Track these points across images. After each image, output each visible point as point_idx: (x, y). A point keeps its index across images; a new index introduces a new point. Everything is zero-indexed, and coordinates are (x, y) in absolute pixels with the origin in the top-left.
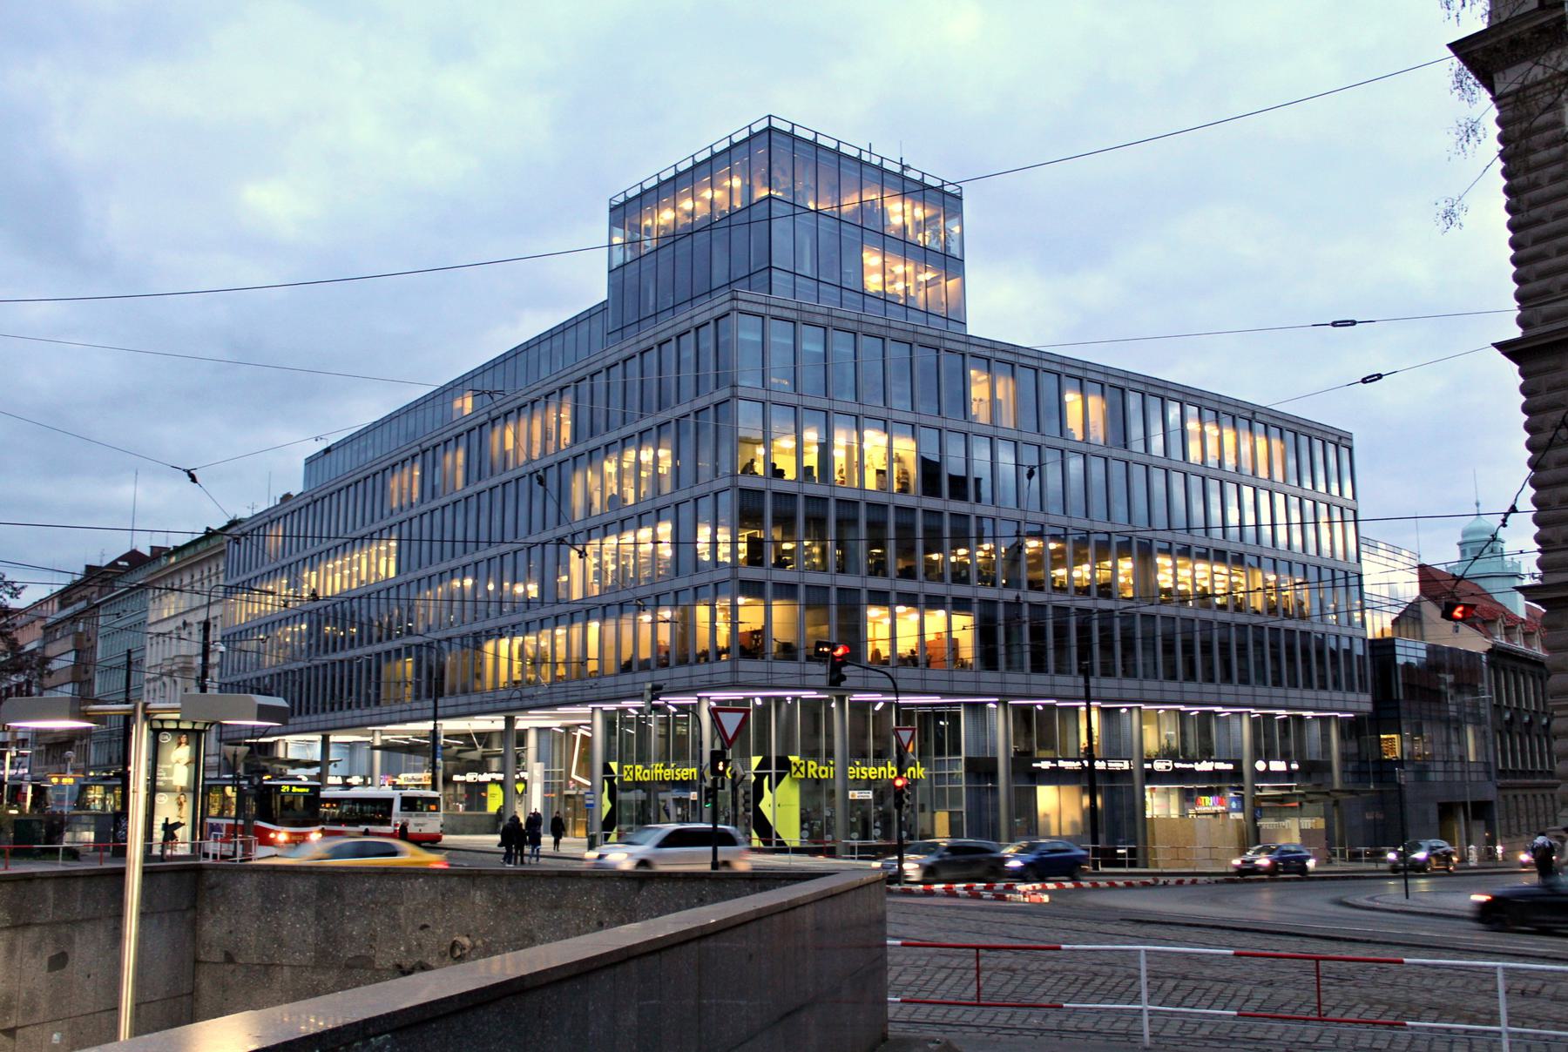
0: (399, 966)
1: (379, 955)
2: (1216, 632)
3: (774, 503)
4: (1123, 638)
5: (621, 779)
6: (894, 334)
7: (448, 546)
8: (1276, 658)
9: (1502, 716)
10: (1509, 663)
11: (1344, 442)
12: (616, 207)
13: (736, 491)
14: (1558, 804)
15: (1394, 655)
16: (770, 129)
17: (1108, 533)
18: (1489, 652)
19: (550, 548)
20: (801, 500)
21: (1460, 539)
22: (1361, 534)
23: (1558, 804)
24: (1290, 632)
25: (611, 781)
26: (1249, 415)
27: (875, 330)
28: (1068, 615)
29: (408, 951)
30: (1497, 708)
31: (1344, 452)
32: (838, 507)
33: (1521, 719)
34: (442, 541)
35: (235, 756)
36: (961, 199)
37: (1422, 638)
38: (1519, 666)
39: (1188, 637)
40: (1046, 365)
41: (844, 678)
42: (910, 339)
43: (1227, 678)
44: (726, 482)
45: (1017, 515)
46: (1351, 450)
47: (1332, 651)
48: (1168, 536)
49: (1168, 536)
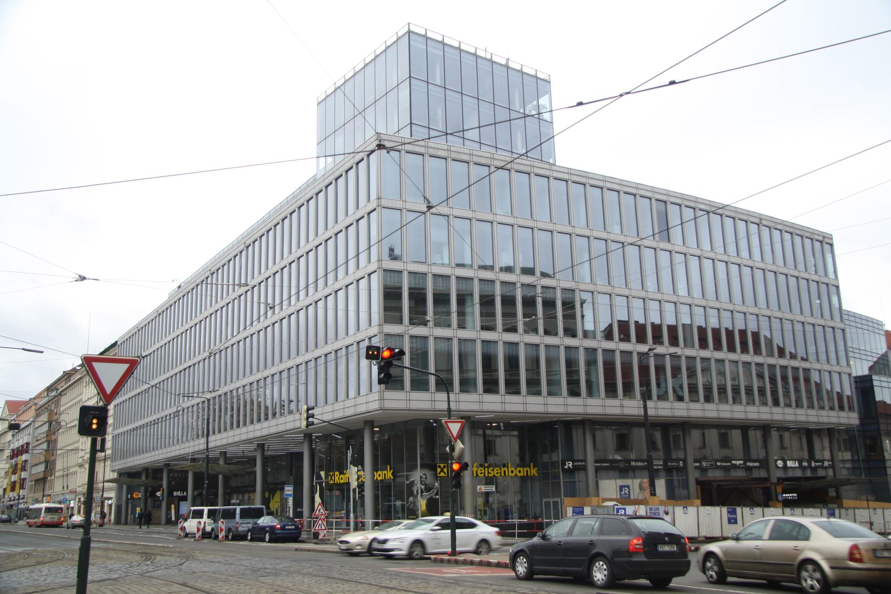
5: (327, 483)
11: (827, 240)
13: (381, 273)
14: (723, 431)
16: (409, 32)
23: (723, 431)
24: (795, 369)
25: (321, 484)
26: (757, 221)
36: (549, 82)
44: (374, 266)
46: (831, 245)
47: (838, 393)
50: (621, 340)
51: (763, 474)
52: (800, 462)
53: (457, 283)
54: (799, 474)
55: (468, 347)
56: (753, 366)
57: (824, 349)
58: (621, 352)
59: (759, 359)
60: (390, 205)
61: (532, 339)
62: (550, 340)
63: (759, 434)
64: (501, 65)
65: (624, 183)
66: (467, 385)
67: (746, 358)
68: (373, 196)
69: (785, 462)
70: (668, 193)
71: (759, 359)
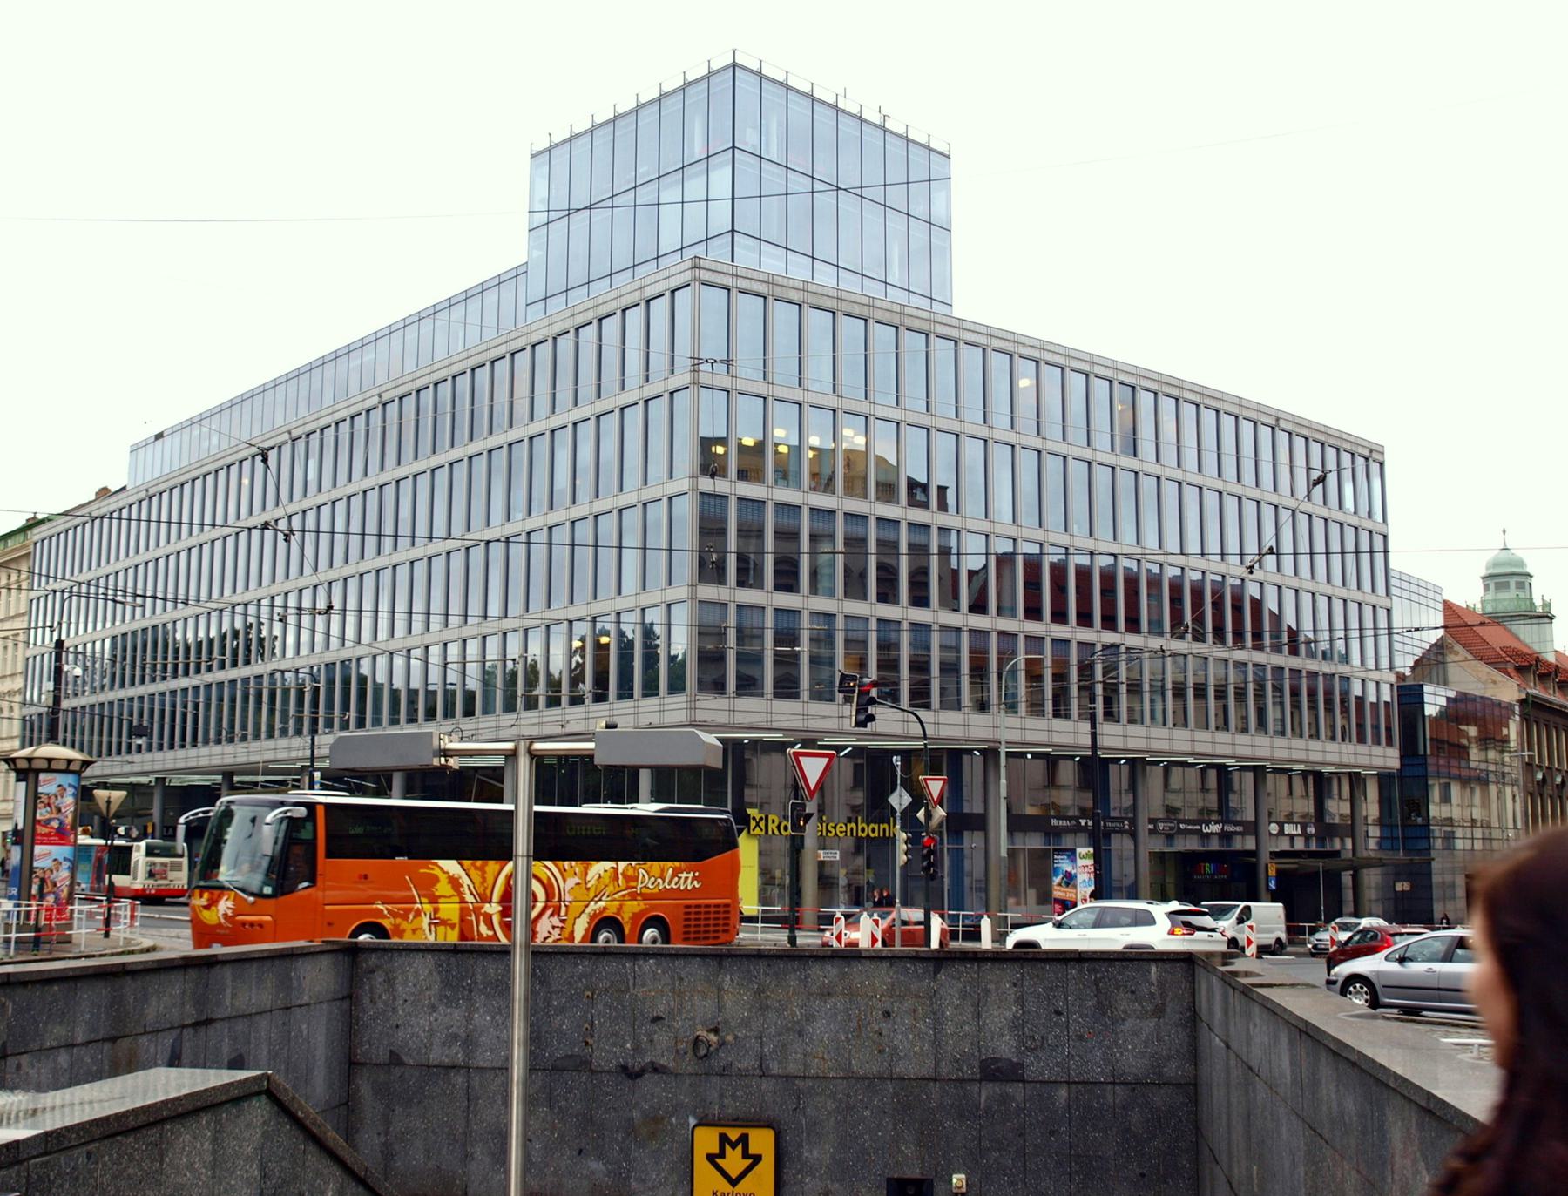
0: (624, 1069)
1: (597, 1054)
2: (1147, 665)
3: (739, 510)
4: (1326, 693)
6: (879, 315)
7: (185, 528)
8: (1313, 706)
9: (1533, 776)
10: (1543, 715)
11: (1375, 455)
12: (539, 153)
13: (696, 496)
15: (1422, 703)
16: (734, 66)
17: (1115, 556)
18: (1522, 702)
19: (256, 534)
20: (770, 508)
21: (1484, 573)
22: (1392, 565)
24: (1313, 675)
26: (1272, 422)
27: (857, 310)
28: (1117, 655)
29: (636, 1048)
30: (1529, 766)
31: (1375, 467)
32: (776, 512)
33: (1553, 780)
34: (180, 523)
35: (109, 802)
37: (1445, 683)
38: (1552, 718)
39: (951, 656)
40: (1049, 357)
41: (871, 718)
42: (896, 321)
43: (1225, 726)
45: (985, 526)
46: (1382, 464)
48: (1181, 560)
49: (1181, 560)
50: (778, 587)
51: (1250, 844)
52: (1304, 828)
53: (811, 519)
54: (1299, 845)
55: (751, 620)
56: (1250, 668)
57: (311, 462)
58: (1079, 643)
59: (1259, 657)
60: (750, 390)
61: (822, 604)
62: (748, 596)
63: (1249, 776)
64: (875, 125)
65: (1072, 354)
66: (748, 685)
67: (1241, 655)
68: (683, 362)
69: (1281, 825)
70: (1138, 373)
71: (1259, 657)
